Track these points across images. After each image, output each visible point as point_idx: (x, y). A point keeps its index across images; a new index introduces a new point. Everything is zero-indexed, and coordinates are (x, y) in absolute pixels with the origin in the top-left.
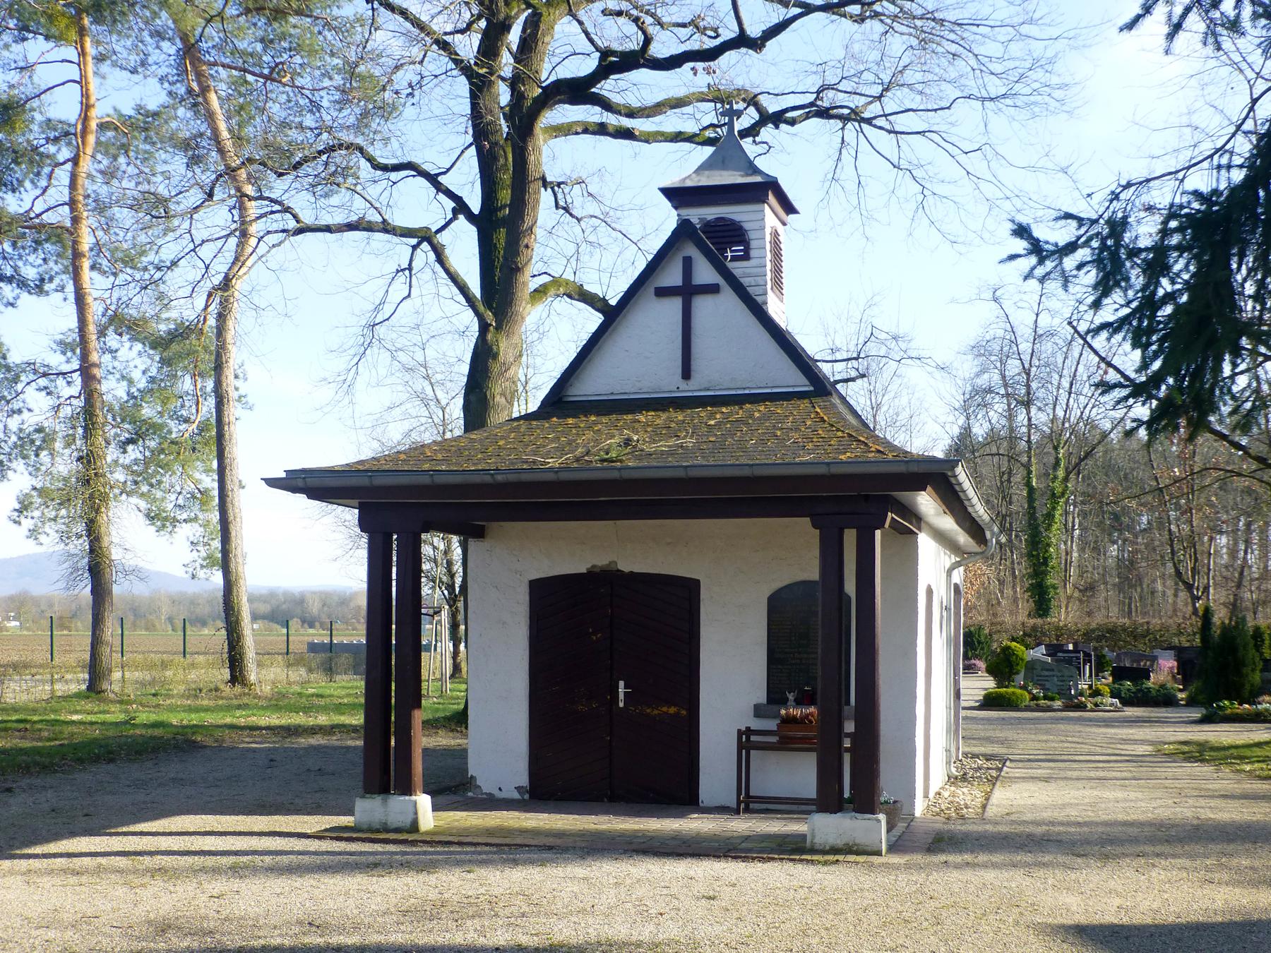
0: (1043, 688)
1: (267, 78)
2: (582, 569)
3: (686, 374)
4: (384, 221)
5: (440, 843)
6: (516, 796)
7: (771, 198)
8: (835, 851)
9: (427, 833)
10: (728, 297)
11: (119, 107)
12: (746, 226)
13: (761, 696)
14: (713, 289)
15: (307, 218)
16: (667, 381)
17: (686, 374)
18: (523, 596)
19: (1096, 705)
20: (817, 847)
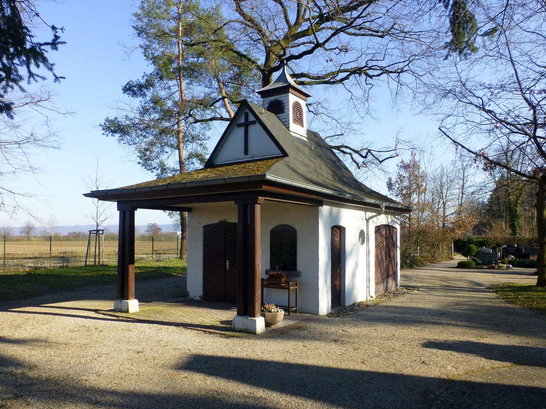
0: (482, 260)
1: (240, 85)
2: (216, 221)
3: (246, 152)
4: (222, 117)
5: (449, 289)
6: (199, 299)
7: (291, 90)
8: (241, 331)
9: (132, 314)
10: (258, 125)
11: (53, 81)
12: (284, 101)
13: (268, 267)
14: (253, 123)
15: (198, 118)
16: (241, 156)
17: (246, 152)
18: (201, 231)
19: (500, 267)
20: (236, 329)
